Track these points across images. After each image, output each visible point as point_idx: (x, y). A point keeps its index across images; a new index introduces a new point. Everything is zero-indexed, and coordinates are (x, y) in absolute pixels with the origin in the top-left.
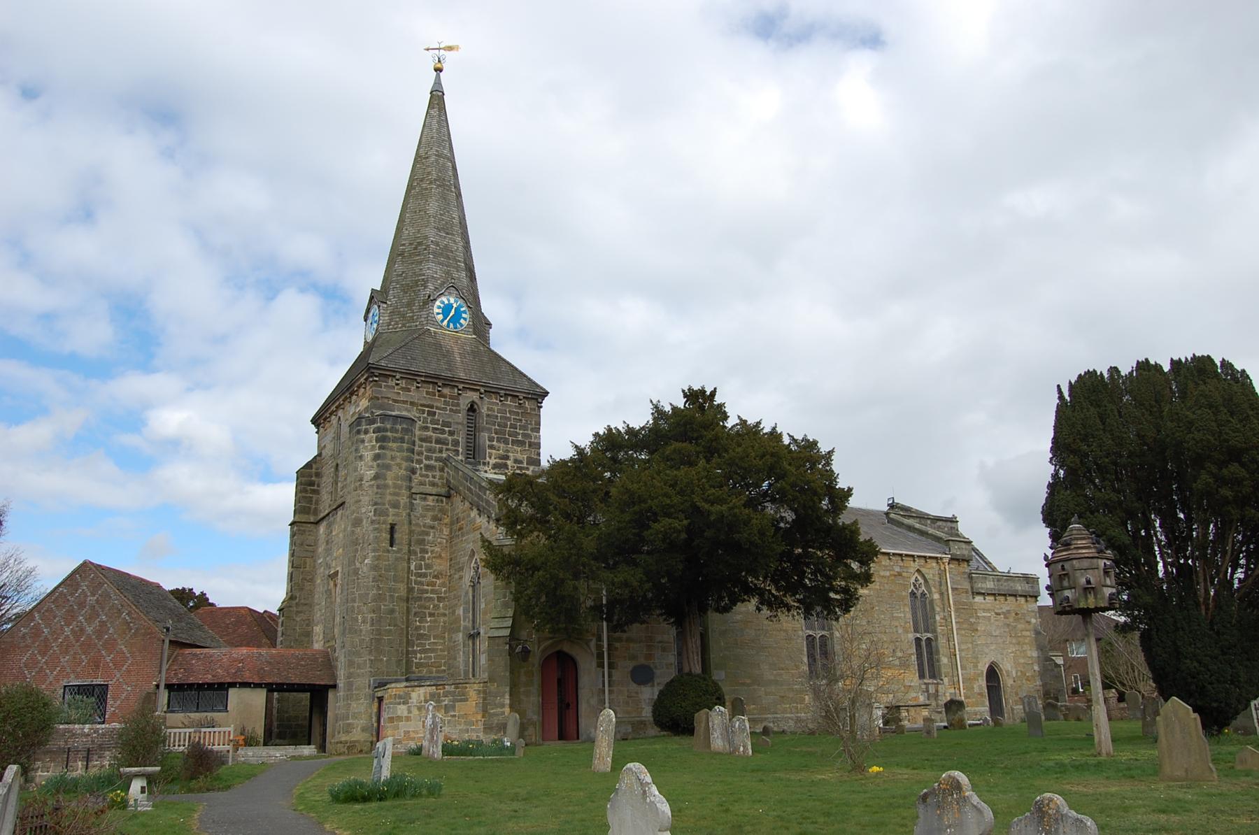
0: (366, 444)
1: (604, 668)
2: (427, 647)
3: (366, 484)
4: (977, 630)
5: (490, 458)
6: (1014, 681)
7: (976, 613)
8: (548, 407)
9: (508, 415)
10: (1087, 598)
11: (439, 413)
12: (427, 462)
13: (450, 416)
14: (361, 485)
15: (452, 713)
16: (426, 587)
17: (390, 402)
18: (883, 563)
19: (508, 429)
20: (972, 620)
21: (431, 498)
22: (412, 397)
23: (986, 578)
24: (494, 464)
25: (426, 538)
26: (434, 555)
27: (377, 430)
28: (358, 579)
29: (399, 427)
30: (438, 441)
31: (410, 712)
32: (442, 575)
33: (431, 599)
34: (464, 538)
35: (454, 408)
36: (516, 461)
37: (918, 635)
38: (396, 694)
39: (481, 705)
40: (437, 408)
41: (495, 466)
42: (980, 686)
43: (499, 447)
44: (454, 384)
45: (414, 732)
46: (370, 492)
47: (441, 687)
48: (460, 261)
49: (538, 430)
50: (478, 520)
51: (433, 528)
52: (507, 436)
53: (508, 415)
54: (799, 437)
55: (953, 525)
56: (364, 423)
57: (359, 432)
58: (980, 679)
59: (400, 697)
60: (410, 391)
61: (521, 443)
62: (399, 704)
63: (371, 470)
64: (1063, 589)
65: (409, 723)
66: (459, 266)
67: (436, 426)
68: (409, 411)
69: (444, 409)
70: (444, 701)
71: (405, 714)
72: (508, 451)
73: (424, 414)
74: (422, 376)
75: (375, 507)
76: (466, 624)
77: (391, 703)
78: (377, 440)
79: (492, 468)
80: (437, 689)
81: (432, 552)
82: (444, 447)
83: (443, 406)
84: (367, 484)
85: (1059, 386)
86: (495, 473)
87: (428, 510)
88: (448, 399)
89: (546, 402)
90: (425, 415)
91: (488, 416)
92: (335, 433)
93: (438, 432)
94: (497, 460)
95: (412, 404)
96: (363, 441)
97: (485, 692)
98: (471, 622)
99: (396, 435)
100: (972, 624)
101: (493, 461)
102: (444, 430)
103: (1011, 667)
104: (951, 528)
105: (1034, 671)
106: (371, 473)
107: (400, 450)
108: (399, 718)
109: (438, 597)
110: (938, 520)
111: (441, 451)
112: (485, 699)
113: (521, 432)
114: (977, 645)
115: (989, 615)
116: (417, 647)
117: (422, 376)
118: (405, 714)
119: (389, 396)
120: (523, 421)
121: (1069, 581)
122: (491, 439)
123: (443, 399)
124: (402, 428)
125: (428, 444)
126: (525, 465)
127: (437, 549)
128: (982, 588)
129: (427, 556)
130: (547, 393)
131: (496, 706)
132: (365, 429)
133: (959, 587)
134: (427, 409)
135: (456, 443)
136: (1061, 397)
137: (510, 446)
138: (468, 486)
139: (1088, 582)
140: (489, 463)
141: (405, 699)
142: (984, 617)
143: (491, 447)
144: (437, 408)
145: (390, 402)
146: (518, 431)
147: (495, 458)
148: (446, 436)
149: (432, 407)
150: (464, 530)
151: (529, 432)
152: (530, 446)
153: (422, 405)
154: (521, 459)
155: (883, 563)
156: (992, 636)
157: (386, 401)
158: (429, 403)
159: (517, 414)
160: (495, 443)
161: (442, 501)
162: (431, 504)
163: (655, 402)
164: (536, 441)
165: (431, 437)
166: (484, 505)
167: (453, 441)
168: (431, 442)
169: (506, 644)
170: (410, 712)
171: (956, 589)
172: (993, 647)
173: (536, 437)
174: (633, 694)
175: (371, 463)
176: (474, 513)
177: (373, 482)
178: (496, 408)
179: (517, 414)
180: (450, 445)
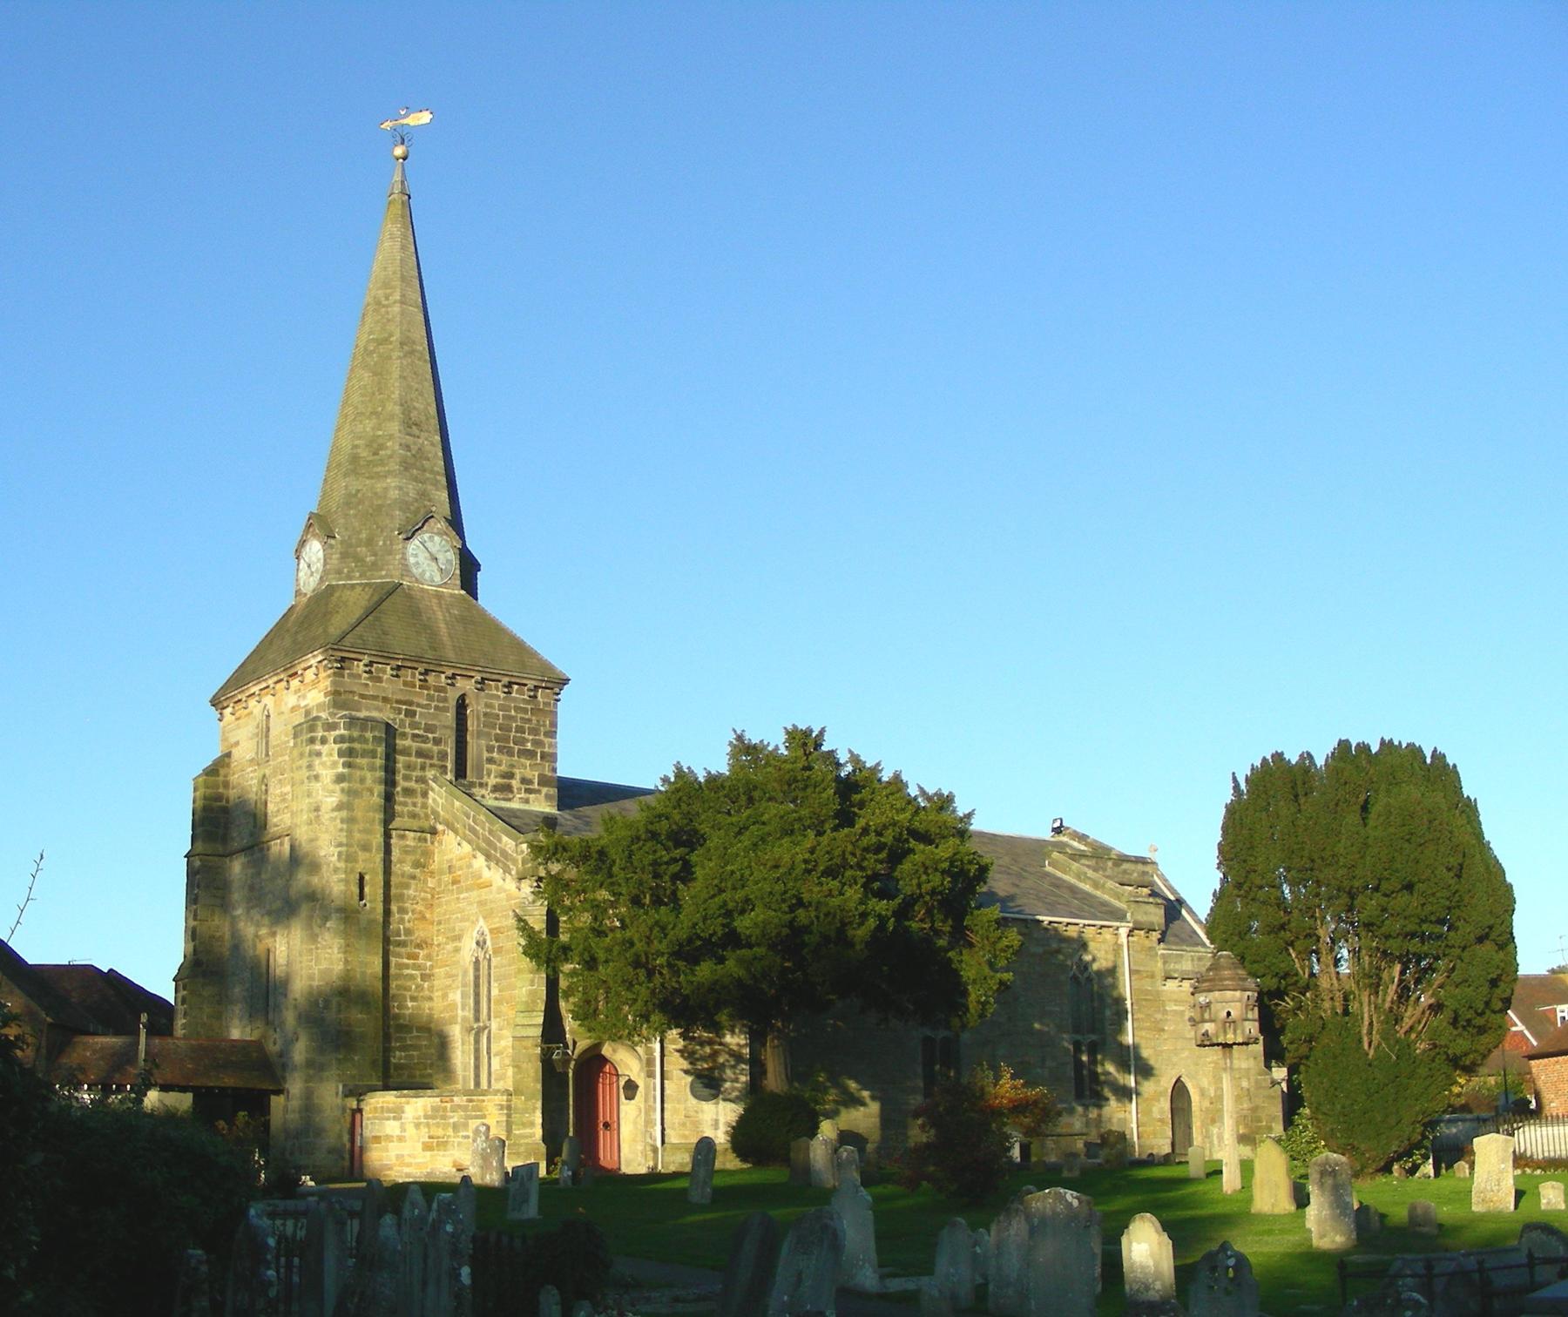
0: (324, 759)
1: (654, 1078)
2: (409, 1042)
3: (326, 815)
4: (1163, 1030)
5: (489, 775)
6: (1211, 1103)
7: (1164, 1006)
8: (568, 705)
9: (513, 713)
10: (1225, 1033)
11: (421, 713)
12: (407, 784)
13: (434, 717)
14: (318, 817)
15: (464, 1134)
16: (406, 961)
17: (356, 698)
18: (1035, 936)
19: (513, 734)
20: (1159, 1016)
21: (411, 834)
22: (384, 690)
23: (1181, 956)
24: (494, 786)
25: (405, 891)
26: (416, 916)
27: (340, 740)
28: (317, 948)
29: (369, 735)
30: (420, 754)
31: (403, 1129)
32: (426, 943)
33: (412, 977)
34: (462, 896)
35: (441, 705)
36: (524, 781)
37: (1079, 1037)
38: (382, 1107)
39: (504, 1124)
40: (419, 705)
41: (496, 788)
42: (1162, 1111)
43: (501, 761)
44: (440, 669)
45: (409, 1155)
46: (331, 828)
47: (448, 1099)
48: (438, 473)
49: (552, 734)
50: (486, 874)
51: (414, 877)
52: (512, 745)
53: (513, 713)
54: (931, 791)
55: (1148, 868)
56: (320, 728)
57: (312, 741)
58: (1162, 1099)
59: (389, 1111)
60: (381, 682)
61: (530, 754)
62: (388, 1119)
63: (331, 796)
64: (1204, 1021)
65: (403, 1144)
66: (437, 481)
67: (416, 732)
68: (380, 710)
69: (427, 707)
70: (453, 1117)
71: (397, 1132)
72: (512, 766)
73: (400, 713)
74: (398, 659)
75: (339, 849)
76: (467, 1014)
77: (375, 1118)
78: (341, 754)
79: (492, 791)
80: (442, 1101)
81: (413, 911)
82: (428, 761)
83: (425, 702)
84: (327, 816)
85: (1234, 774)
86: (496, 799)
87: (406, 852)
88: (432, 692)
89: (566, 693)
90: (402, 716)
91: (486, 714)
92: (258, 727)
93: (420, 740)
94: (499, 780)
95: (385, 700)
96: (319, 754)
97: (509, 1108)
98: (472, 1012)
99: (365, 746)
100: (1157, 1022)
101: (492, 781)
102: (428, 738)
103: (1209, 1083)
104: (1143, 872)
105: (1242, 1088)
106: (332, 801)
107: (372, 768)
108: (389, 1138)
109: (421, 975)
110: (1124, 861)
111: (423, 768)
112: (509, 1116)
113: (531, 737)
114: (1162, 1052)
115: (1182, 1008)
116: (396, 1041)
117: (398, 659)
118: (397, 1132)
119: (355, 689)
120: (534, 722)
121: (1210, 1014)
122: (490, 749)
123: (426, 692)
124: (374, 737)
125: (407, 758)
126: (536, 786)
127: (419, 908)
128: (1176, 971)
129: (407, 917)
130: (566, 681)
131: (524, 1125)
132: (322, 737)
133: (1142, 969)
134: (404, 707)
135: (443, 756)
136: (1236, 787)
137: (516, 758)
138: (469, 825)
139: (1229, 1014)
140: (487, 785)
141: (397, 1113)
142: (1175, 1011)
143: (490, 761)
144: (419, 705)
145: (356, 698)
146: (526, 736)
147: (496, 777)
148: (429, 745)
149: (410, 703)
150: (462, 884)
151: (542, 737)
152: (542, 758)
153: (398, 702)
154: (531, 777)
155: (1035, 936)
156: (1186, 1039)
157: (351, 696)
158: (407, 698)
159: (525, 711)
160: (495, 755)
161: (425, 840)
162: (412, 844)
163: (739, 732)
164: (551, 751)
165: (410, 747)
166: (498, 855)
167: (439, 752)
168: (409, 755)
169: (536, 1046)
170: (403, 1129)
171: (1138, 972)
172: (1186, 1054)
173: (551, 745)
174: (692, 1114)
175: (332, 787)
176: (480, 861)
177: (336, 814)
178: (496, 703)
179: (525, 711)
180: (436, 758)
